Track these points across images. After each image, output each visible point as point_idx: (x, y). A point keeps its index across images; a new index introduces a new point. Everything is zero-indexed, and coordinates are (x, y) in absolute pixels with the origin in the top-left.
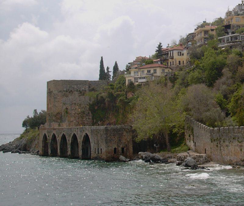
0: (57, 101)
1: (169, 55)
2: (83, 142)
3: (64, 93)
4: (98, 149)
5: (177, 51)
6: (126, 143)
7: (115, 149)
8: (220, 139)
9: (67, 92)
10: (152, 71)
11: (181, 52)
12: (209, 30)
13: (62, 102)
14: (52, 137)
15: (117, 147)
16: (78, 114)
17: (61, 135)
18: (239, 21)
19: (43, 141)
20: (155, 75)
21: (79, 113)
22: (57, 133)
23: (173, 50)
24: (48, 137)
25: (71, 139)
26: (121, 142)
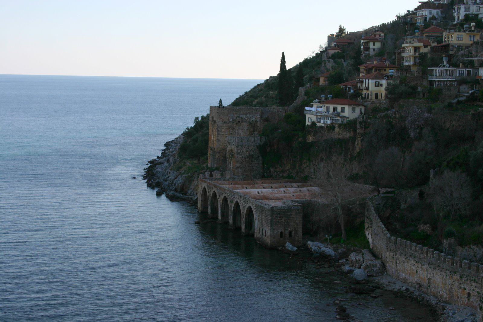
0: (221, 135)
1: (364, 85)
2: (246, 215)
6: (295, 225)
7: (281, 233)
9: (233, 123)
10: (339, 110)
11: (379, 82)
12: (421, 46)
13: (227, 135)
14: (212, 194)
15: (283, 231)
16: (245, 158)
17: (222, 197)
18: (462, 39)
19: (202, 195)
21: (246, 157)
22: (218, 193)
24: (209, 192)
25: (233, 206)
26: (288, 224)
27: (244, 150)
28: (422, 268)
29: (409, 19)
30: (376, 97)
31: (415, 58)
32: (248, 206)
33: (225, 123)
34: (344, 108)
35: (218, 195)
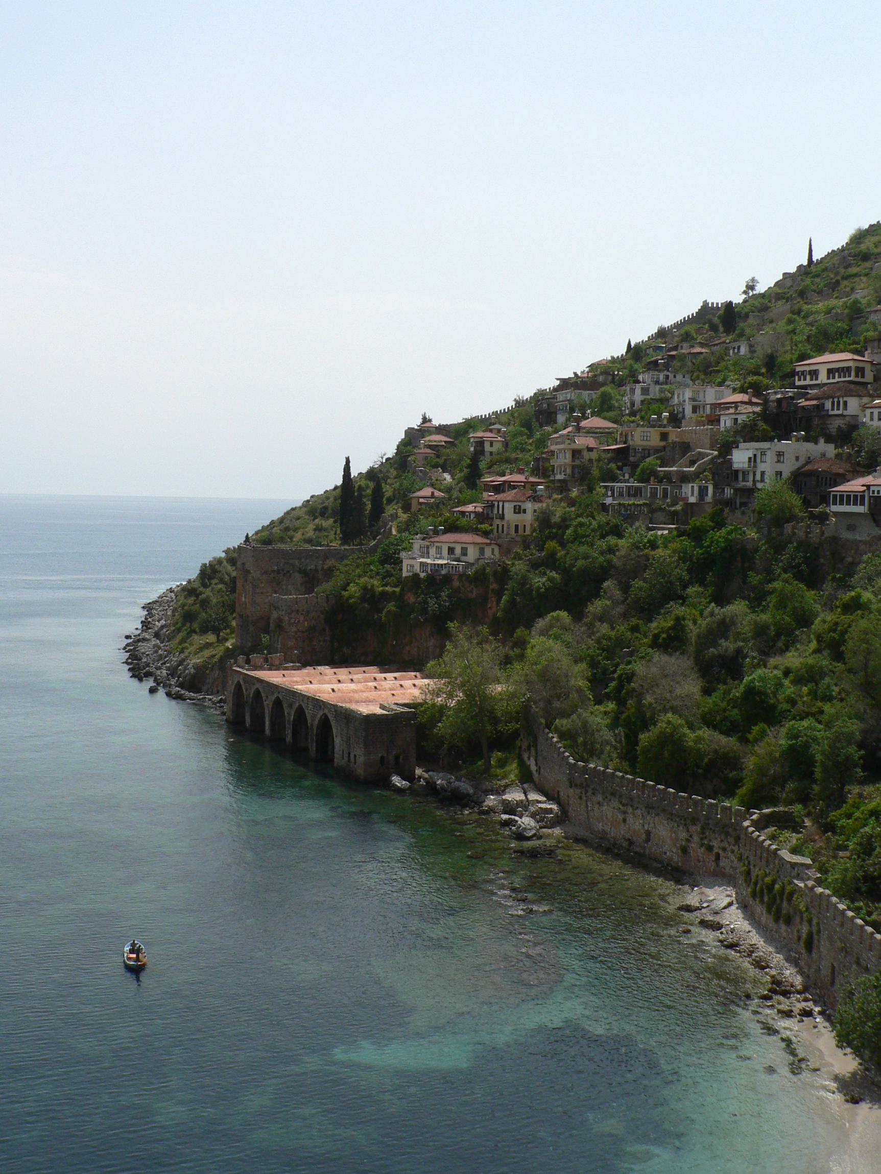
1: (495, 512)
2: (317, 728)
3: (272, 575)
4: (349, 754)
5: (513, 504)
7: (382, 758)
8: (588, 786)
11: (520, 506)
20: (463, 558)
23: (504, 502)
25: (293, 713)
27: (302, 618)
28: (634, 814)
29: (545, 406)
30: (517, 530)
31: (573, 467)
32: (321, 713)
33: (266, 573)
34: (466, 549)
35: (263, 695)
